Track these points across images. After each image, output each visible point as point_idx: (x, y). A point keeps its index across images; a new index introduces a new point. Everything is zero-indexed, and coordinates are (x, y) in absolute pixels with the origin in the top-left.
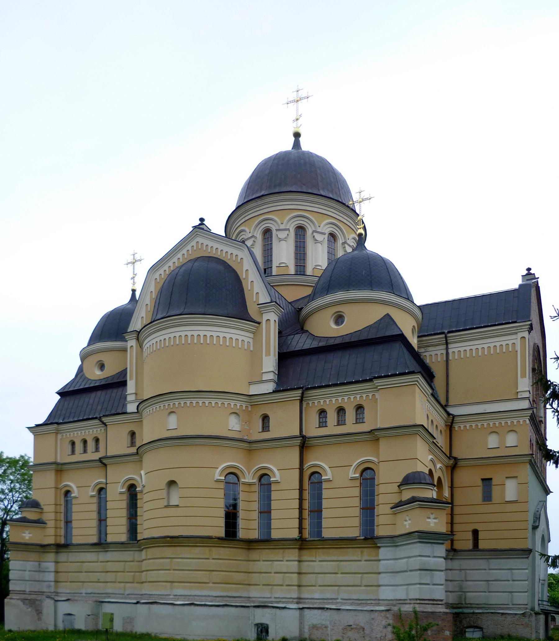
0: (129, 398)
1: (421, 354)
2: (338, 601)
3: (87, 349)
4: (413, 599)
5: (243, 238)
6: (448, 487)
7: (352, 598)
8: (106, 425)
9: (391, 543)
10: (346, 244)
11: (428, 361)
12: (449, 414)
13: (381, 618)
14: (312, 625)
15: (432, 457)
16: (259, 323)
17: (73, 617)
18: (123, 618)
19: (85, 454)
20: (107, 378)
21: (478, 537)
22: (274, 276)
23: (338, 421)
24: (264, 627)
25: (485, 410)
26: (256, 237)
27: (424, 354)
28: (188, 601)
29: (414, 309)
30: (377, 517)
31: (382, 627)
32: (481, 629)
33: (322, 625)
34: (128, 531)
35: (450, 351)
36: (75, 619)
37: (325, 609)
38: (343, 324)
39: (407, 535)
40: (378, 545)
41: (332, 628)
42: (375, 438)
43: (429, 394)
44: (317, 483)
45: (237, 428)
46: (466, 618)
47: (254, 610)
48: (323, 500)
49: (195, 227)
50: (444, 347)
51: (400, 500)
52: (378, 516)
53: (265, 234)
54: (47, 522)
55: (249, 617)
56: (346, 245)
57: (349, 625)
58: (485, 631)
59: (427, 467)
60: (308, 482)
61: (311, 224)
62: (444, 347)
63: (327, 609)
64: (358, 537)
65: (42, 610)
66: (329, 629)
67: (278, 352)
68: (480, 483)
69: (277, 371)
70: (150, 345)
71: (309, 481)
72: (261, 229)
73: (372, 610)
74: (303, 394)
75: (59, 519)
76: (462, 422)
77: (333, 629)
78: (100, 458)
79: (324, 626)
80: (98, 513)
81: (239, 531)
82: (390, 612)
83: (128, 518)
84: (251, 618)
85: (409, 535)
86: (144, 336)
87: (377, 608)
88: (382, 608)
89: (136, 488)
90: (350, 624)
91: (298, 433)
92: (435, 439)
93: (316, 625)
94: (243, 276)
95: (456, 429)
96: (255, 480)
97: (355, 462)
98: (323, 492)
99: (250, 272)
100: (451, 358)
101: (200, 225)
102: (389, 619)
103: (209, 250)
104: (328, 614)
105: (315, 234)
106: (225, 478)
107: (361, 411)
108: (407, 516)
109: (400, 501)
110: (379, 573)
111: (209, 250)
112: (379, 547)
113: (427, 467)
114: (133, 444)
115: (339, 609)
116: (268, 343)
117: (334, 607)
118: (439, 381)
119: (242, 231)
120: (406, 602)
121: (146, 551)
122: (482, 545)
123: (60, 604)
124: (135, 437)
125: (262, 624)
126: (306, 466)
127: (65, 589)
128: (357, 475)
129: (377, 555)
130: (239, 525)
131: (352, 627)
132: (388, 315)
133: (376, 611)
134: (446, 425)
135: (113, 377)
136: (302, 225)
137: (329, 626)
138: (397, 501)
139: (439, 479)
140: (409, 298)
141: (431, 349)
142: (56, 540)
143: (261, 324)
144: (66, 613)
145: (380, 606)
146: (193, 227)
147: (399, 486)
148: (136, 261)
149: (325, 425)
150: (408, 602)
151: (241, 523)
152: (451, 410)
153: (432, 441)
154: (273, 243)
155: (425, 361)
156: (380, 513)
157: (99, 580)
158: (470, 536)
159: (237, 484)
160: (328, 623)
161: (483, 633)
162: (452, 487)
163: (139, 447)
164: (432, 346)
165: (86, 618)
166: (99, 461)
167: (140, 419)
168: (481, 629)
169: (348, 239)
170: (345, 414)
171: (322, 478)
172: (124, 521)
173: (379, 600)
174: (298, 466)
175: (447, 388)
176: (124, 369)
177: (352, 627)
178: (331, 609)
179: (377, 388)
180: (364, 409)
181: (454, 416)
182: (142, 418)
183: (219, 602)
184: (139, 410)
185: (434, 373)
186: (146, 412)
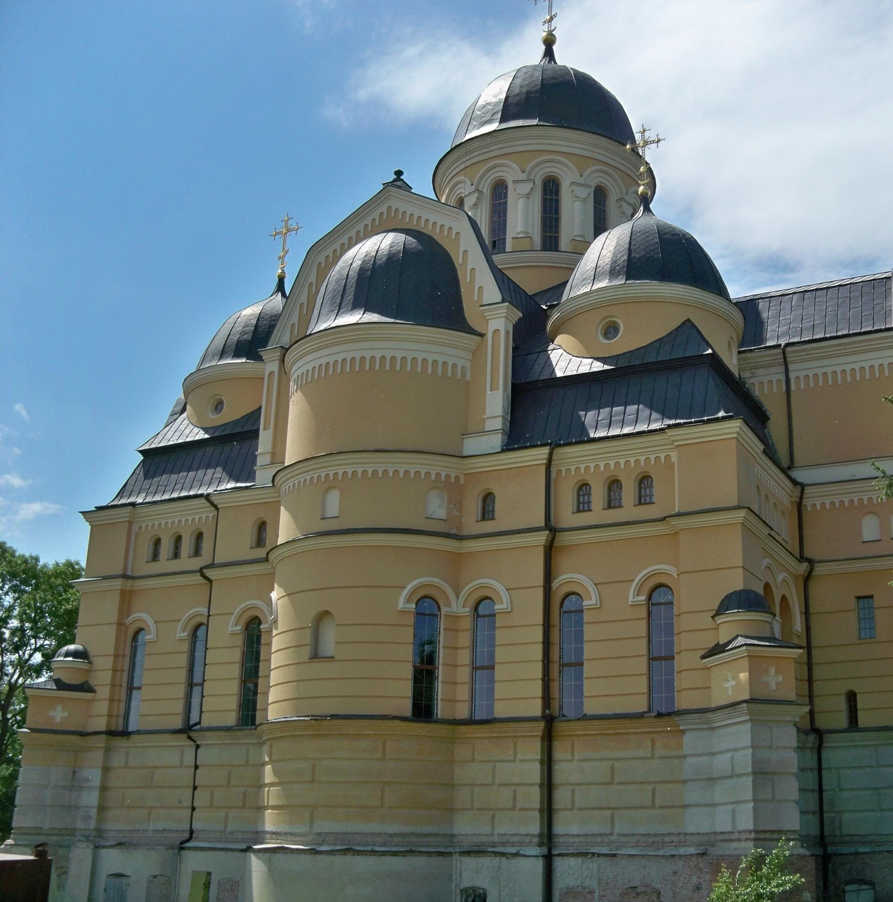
0: (260, 461)
1: (746, 381)
2: (612, 838)
3: (196, 375)
4: (745, 832)
5: (460, 193)
6: (801, 613)
7: (637, 832)
8: (217, 509)
9: (702, 724)
10: (623, 202)
11: (757, 392)
12: (795, 483)
13: (689, 870)
14: (565, 890)
15: (770, 562)
16: (482, 335)
17: (125, 880)
18: (219, 881)
19: (175, 561)
20: (225, 424)
21: (856, 706)
22: (508, 252)
23: (610, 501)
24: (480, 895)
25: (854, 476)
26: (481, 192)
27: (752, 381)
28: (342, 845)
29: (731, 311)
30: (678, 617)
31: (692, 888)
32: (871, 884)
33: (584, 888)
34: (240, 706)
35: (792, 376)
36: (129, 885)
37: (590, 856)
38: (617, 336)
39: (729, 709)
40: (681, 728)
41: (602, 893)
42: (672, 530)
43: (759, 452)
44: (574, 612)
45: (442, 513)
46: (843, 864)
47: (461, 861)
48: (584, 643)
49: (386, 185)
50: (782, 369)
51: (716, 643)
52: (679, 691)
53: (495, 188)
54: (96, 688)
55: (452, 875)
56: (624, 204)
57: (632, 886)
58: (878, 888)
59: (761, 580)
60: (559, 611)
61: (565, 169)
62: (782, 369)
63: (593, 854)
64: (646, 712)
65: (67, 868)
66: (596, 895)
67: (512, 383)
68: (853, 603)
69: (509, 415)
70: (303, 373)
71: (560, 610)
72: (489, 181)
73: (673, 856)
74: (551, 454)
75: (115, 713)
76: (818, 497)
77: (604, 896)
78: (201, 569)
79: (587, 890)
80: (189, 671)
81: (437, 704)
82: (705, 857)
83: (242, 681)
84: (454, 876)
85: (733, 708)
86: (293, 357)
87: (682, 851)
88: (692, 850)
89: (260, 623)
90: (634, 886)
91: (542, 523)
92: (772, 529)
93: (573, 888)
94: (458, 260)
95: (809, 508)
96: (467, 610)
97: (641, 572)
98: (585, 629)
99: (470, 255)
100: (793, 387)
101: (395, 180)
102: (703, 872)
103: (407, 220)
104: (593, 865)
105: (573, 187)
106: (416, 605)
107: (648, 482)
108: (729, 671)
109: (716, 645)
110: (685, 782)
111: (407, 220)
112: (683, 732)
113: (761, 580)
114: (260, 542)
115: (615, 855)
116: (494, 370)
117: (605, 851)
118: (776, 427)
119: (459, 183)
120: (733, 836)
121: (271, 746)
122: (864, 720)
123: (104, 852)
124: (265, 528)
125: (474, 889)
126: (555, 584)
127: (115, 825)
128: (643, 598)
129: (680, 747)
130: (437, 692)
131: (638, 890)
132: (689, 320)
133: (680, 856)
134: (792, 502)
135: (236, 422)
136: (551, 174)
137: (597, 891)
138: (711, 645)
139: (784, 599)
140: (720, 289)
141: (761, 371)
142: (108, 724)
143: (485, 336)
144: (112, 873)
145: (687, 846)
146: (383, 184)
147: (713, 617)
148: (288, 231)
149: (588, 507)
150: (736, 836)
151: (440, 690)
152: (800, 475)
153: (767, 534)
154: (507, 239)
155: (752, 392)
156: (682, 611)
157: (180, 802)
158: (842, 704)
159: (437, 616)
160: (594, 884)
161: (876, 892)
162: (807, 613)
163: (272, 549)
164: (762, 367)
165: (149, 881)
166: (199, 574)
167: (276, 497)
168: (871, 884)
169: (627, 194)
170: (621, 488)
171: (583, 604)
172: (234, 687)
173: (685, 834)
174: (541, 582)
175: (789, 422)
176: (257, 408)
177: (638, 890)
178: (599, 855)
179: (673, 444)
180: (652, 480)
181: (803, 486)
182: (279, 497)
183: (396, 846)
184: (275, 484)
185: (768, 413)
186: (287, 487)
